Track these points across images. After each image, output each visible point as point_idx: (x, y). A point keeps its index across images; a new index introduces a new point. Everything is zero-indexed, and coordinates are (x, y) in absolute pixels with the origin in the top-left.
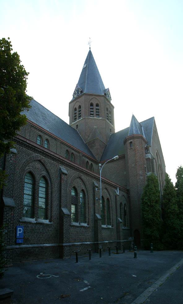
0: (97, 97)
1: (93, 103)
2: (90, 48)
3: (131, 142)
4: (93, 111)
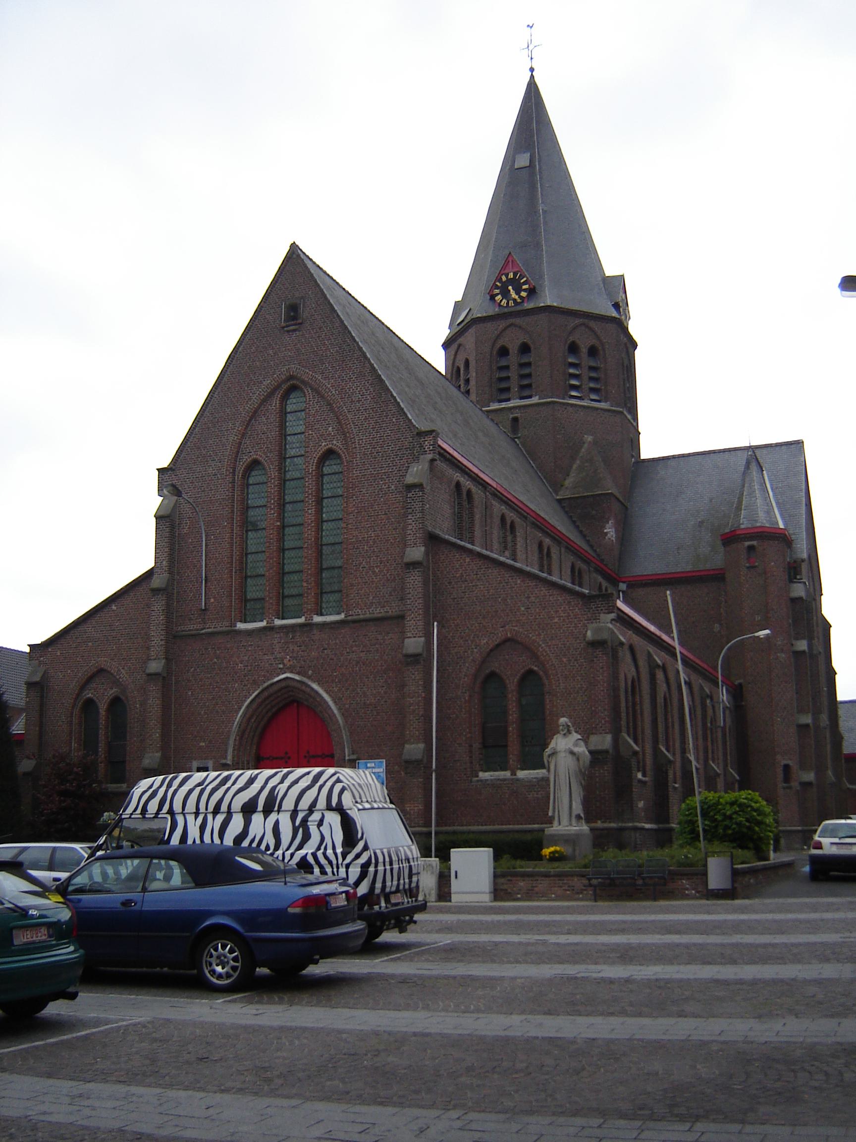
0: (592, 324)
1: (578, 342)
2: (532, 70)
3: (751, 548)
4: (508, 378)
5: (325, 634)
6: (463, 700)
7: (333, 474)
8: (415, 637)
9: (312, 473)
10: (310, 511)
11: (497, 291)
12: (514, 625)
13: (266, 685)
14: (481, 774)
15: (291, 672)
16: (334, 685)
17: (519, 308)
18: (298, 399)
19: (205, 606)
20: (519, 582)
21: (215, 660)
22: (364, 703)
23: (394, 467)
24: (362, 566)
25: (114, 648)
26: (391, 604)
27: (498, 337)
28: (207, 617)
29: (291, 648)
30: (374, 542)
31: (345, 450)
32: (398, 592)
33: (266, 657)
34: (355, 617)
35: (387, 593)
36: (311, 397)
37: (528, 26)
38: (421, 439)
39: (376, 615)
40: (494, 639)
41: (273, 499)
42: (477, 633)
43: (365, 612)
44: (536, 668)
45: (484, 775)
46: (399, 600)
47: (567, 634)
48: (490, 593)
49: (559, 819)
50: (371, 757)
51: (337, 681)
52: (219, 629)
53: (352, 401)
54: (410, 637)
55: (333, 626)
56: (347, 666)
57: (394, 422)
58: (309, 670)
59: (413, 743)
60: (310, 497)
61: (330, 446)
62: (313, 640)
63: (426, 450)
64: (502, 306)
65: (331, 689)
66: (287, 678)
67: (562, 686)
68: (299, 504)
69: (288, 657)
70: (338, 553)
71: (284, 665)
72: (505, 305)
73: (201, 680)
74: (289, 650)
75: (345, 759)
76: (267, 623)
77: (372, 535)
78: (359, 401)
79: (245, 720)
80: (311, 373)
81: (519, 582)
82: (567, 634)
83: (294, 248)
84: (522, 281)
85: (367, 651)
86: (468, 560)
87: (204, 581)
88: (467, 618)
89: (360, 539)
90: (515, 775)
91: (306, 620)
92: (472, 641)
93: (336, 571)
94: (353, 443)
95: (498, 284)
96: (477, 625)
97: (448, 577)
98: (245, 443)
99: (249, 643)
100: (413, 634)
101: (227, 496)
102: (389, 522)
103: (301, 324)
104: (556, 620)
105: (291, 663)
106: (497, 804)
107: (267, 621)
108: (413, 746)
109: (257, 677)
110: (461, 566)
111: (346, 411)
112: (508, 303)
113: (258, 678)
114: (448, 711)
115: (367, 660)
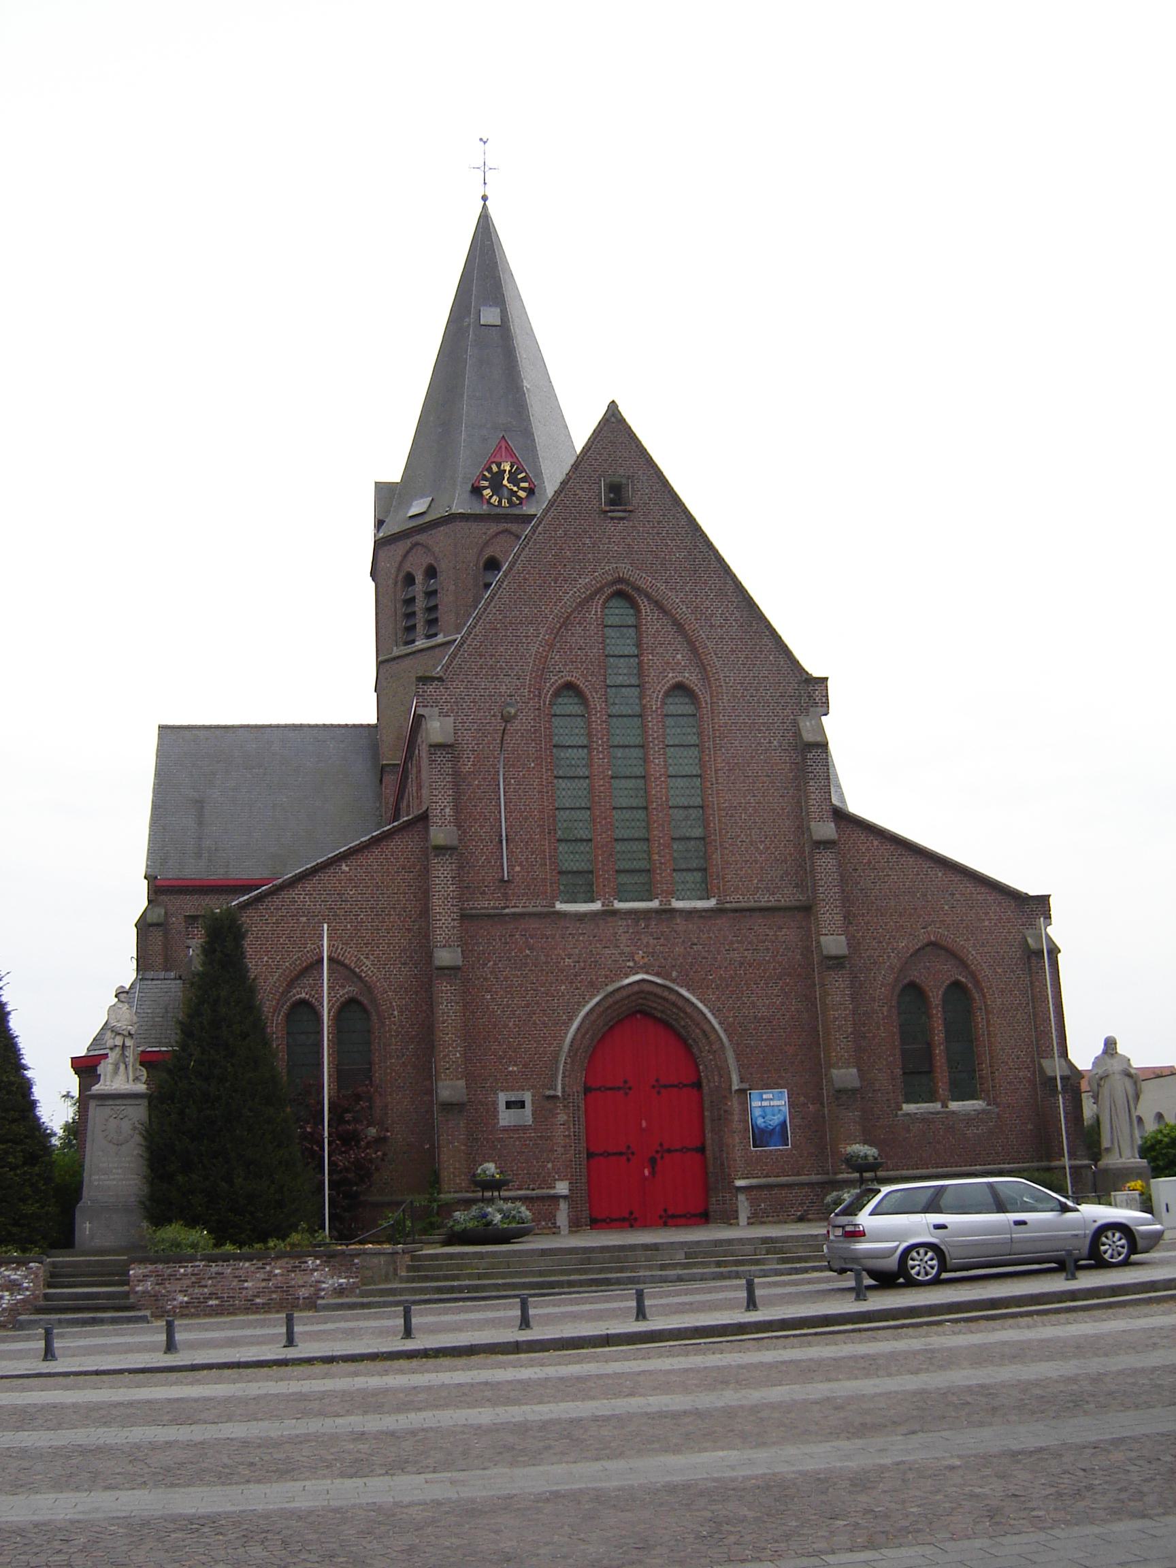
2: (485, 198)
5: (693, 924)
6: (880, 1015)
7: (680, 715)
8: (833, 934)
9: (656, 711)
10: (657, 761)
11: (486, 484)
12: (937, 926)
13: (610, 988)
14: (905, 1106)
15: (647, 973)
16: (710, 991)
17: (516, 511)
18: (622, 610)
19: (508, 876)
20: (940, 874)
21: (527, 951)
22: (755, 1017)
23: (776, 718)
24: (739, 840)
25: (349, 927)
26: (783, 891)
27: (486, 544)
28: (510, 892)
29: (645, 942)
30: (756, 811)
31: (702, 688)
32: (792, 877)
33: (607, 951)
34: (734, 905)
35: (776, 877)
36: (648, 610)
37: (481, 139)
38: (808, 687)
39: (763, 904)
40: (914, 942)
41: (602, 739)
42: (894, 933)
43: (748, 898)
44: (964, 980)
45: (909, 1108)
46: (794, 887)
47: (1000, 940)
48: (907, 886)
49: (1120, 1149)
50: (767, 1087)
51: (713, 986)
52: (531, 909)
53: (712, 626)
54: (826, 935)
55: (703, 914)
56: (726, 967)
57: (771, 661)
58: (672, 971)
59: (842, 1067)
60: (656, 742)
61: (680, 679)
62: (676, 931)
63: (817, 701)
64: (491, 504)
65: (706, 996)
66: (643, 980)
67: (999, 1001)
68: (632, 750)
69: (640, 952)
70: (694, 820)
71: (635, 962)
72: (496, 503)
73: (506, 979)
74: (642, 943)
75: (730, 1089)
76: (603, 906)
77: (752, 801)
78: (721, 626)
79: (579, 1036)
80: (650, 579)
81: (940, 874)
82: (1000, 940)
83: (613, 406)
84: (519, 476)
85: (754, 950)
86: (876, 843)
87: (504, 842)
88: (879, 915)
89: (735, 805)
90: (947, 1107)
91: (661, 905)
92: (888, 944)
93: (692, 843)
94: (716, 680)
95: (486, 473)
96: (891, 923)
97: (851, 863)
98: (551, 658)
99: (580, 931)
100: (829, 931)
101: (532, 727)
102: (772, 786)
103: (630, 511)
104: (987, 923)
105: (646, 960)
106: (929, 1143)
107: (603, 902)
108: (843, 1071)
109: (594, 977)
110: (868, 850)
111: (703, 636)
112: (500, 502)
113: (597, 979)
114: (862, 1029)
115: (754, 960)
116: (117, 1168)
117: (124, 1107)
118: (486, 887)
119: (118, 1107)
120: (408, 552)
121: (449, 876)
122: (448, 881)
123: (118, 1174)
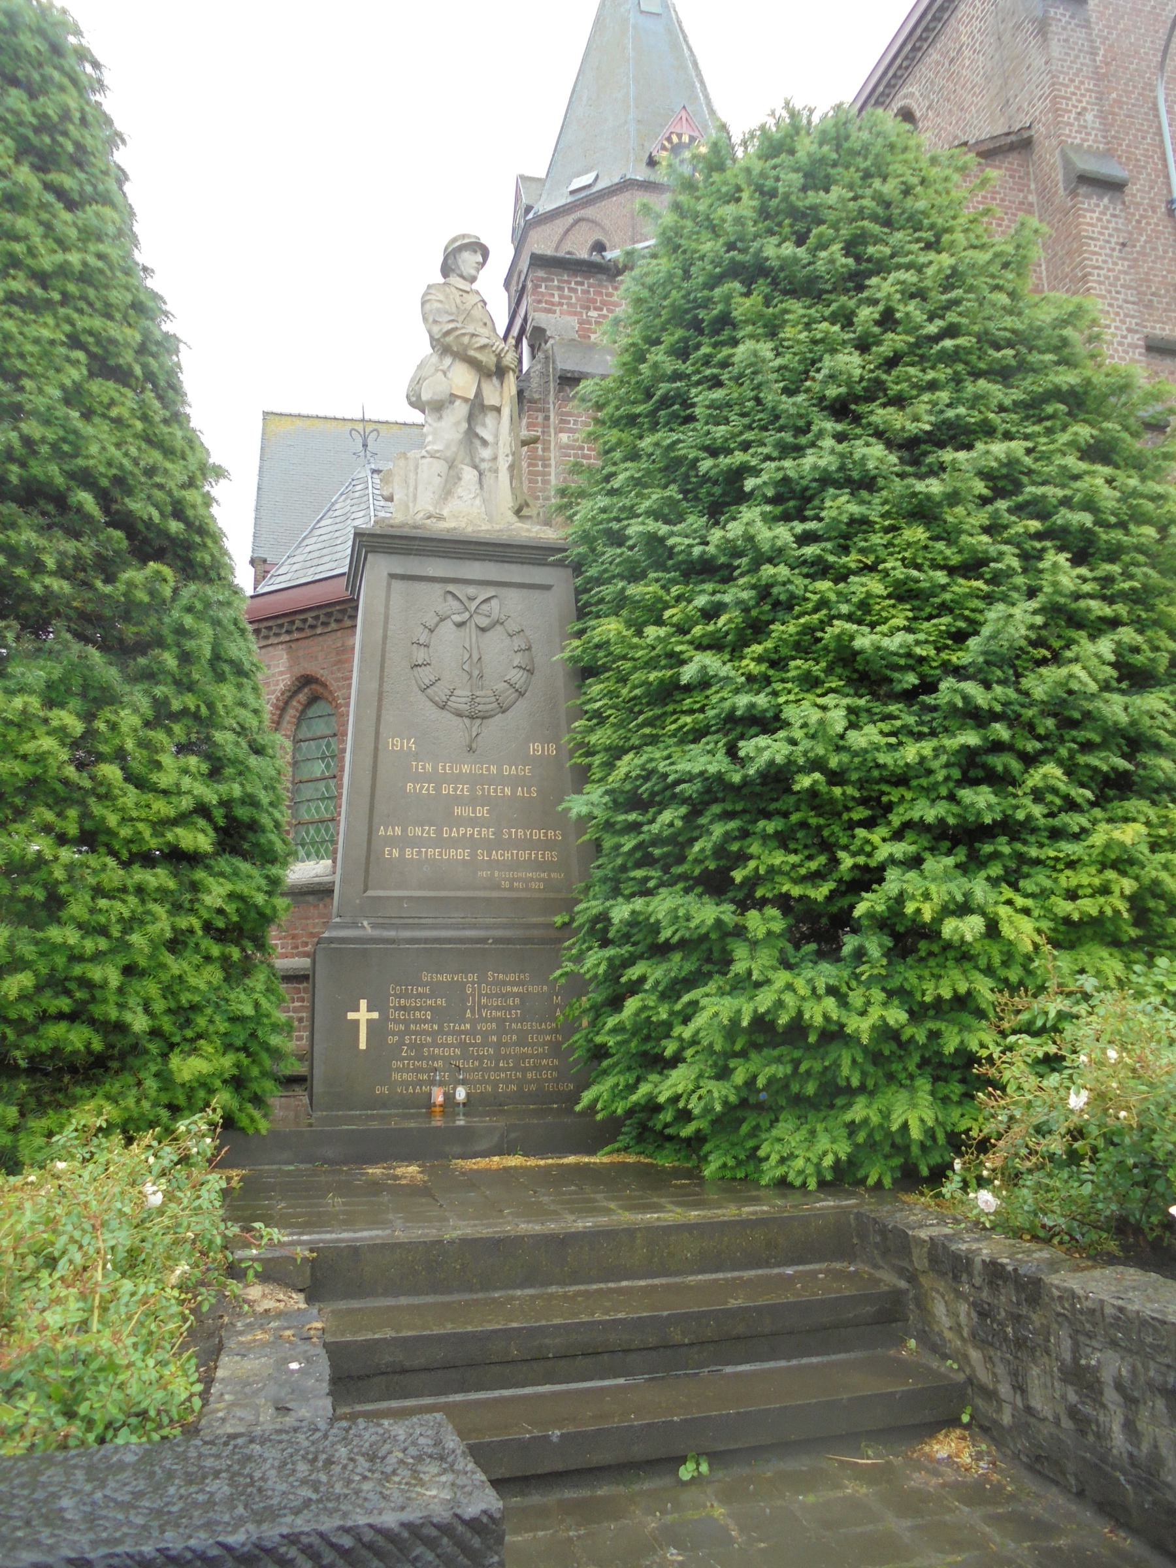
116: (473, 801)
117: (491, 592)
118: (1153, 294)
119: (471, 590)
120: (568, 230)
121: (1114, 240)
122: (1113, 250)
123: (473, 822)
